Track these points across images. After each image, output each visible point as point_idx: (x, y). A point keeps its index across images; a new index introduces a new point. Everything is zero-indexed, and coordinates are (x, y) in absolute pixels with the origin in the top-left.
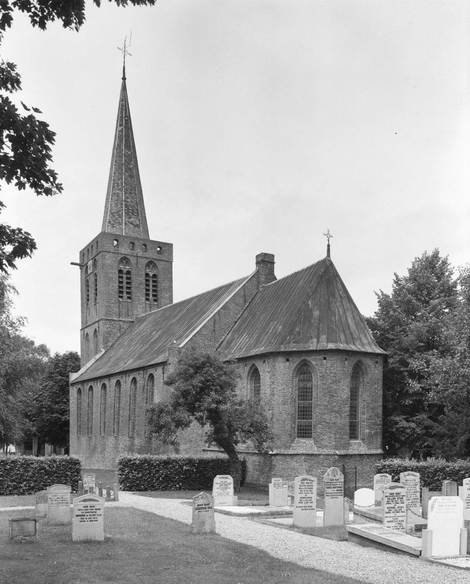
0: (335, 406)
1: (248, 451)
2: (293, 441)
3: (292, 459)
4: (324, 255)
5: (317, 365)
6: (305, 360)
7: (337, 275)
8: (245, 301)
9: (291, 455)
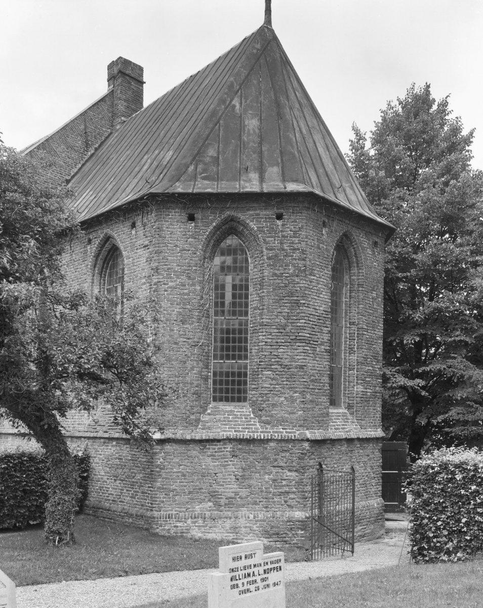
0: (302, 328)
1: (95, 435)
2: (204, 410)
3: (202, 451)
4: (260, 21)
5: (261, 230)
6: (232, 219)
7: (286, 62)
8: (87, 145)
9: (201, 441)
